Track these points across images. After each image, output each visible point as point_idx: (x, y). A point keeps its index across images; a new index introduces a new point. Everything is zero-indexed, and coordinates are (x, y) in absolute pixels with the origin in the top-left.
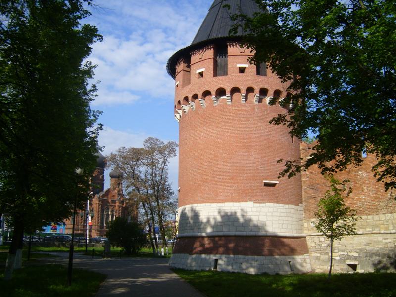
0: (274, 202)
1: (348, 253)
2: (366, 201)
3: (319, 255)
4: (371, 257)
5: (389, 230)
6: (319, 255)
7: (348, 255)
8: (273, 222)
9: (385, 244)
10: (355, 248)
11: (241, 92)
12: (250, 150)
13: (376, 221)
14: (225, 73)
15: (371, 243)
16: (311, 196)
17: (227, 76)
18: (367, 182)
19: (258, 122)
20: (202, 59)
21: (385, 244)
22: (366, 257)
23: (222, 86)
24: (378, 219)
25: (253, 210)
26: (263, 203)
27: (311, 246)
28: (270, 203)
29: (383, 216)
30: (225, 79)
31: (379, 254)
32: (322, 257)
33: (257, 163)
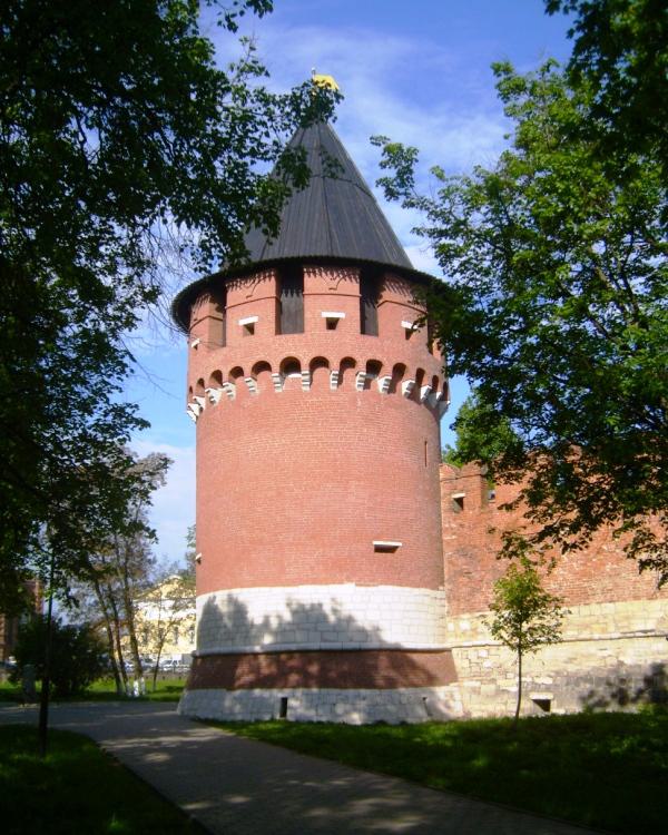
2: (565, 579)
3: (478, 684)
7: (533, 682)
20: (336, 292)
22: (567, 684)
23: (293, 354)
29: (598, 606)
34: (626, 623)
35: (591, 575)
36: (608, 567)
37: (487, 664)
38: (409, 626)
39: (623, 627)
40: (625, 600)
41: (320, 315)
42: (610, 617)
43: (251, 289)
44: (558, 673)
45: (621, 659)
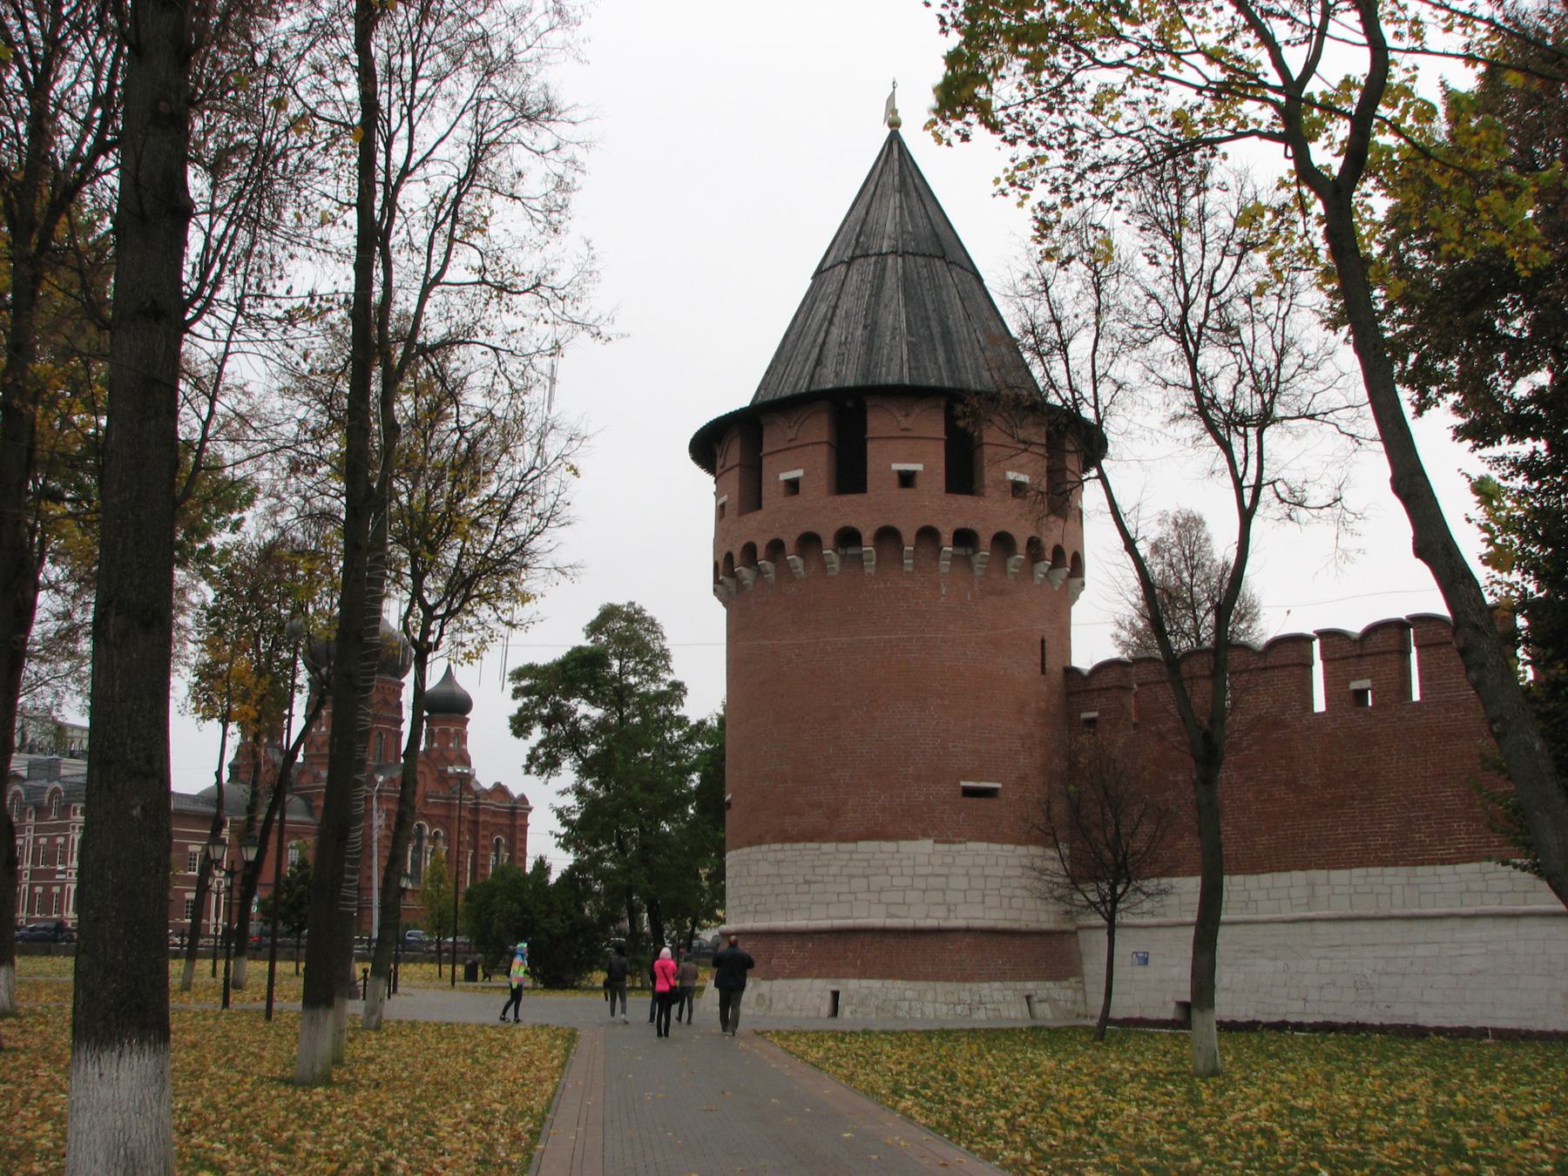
11: (905, 540)
38: (1011, 898)
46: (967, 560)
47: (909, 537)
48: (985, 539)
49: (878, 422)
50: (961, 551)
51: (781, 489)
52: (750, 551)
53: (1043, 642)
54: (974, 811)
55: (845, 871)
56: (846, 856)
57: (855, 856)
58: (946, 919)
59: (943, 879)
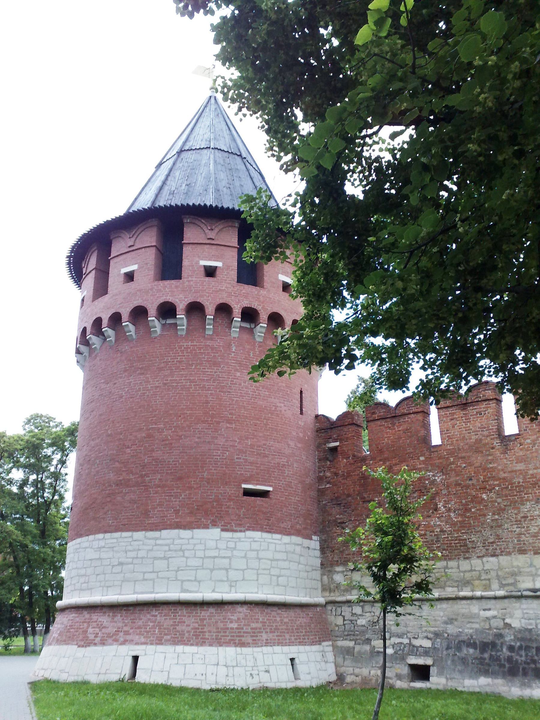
0: (262, 530)
1: (410, 639)
2: (442, 531)
3: (351, 644)
4: (459, 648)
5: (492, 591)
6: (351, 644)
7: (410, 644)
8: (260, 572)
9: (485, 621)
10: (424, 629)
12: (218, 423)
13: (465, 571)
14: (178, 276)
15: (456, 620)
16: (335, 521)
17: (215, 279)
18: (444, 492)
19: (237, 370)
20: (213, 242)
21: (485, 621)
22: (447, 649)
23: (170, 299)
24: (469, 568)
25: (219, 546)
26: (241, 531)
27: (337, 626)
28: (253, 530)
29: (479, 561)
30: (177, 287)
31: (475, 643)
32: (357, 648)
33: (231, 449)
34: (511, 581)
35: (470, 527)
36: (489, 518)
37: (362, 622)
38: (278, 577)
39: (508, 585)
40: (509, 554)
41: (198, 263)
42: (493, 574)
43: (133, 239)
44: (437, 635)
45: (508, 621)
46: (251, 331)
47: (210, 310)
48: (264, 317)
49: (192, 233)
50: (246, 325)
51: (122, 279)
52: (98, 322)
53: (301, 392)
54: (252, 507)
55: (151, 554)
56: (152, 542)
57: (159, 542)
58: (446, 567)
59: (227, 561)
